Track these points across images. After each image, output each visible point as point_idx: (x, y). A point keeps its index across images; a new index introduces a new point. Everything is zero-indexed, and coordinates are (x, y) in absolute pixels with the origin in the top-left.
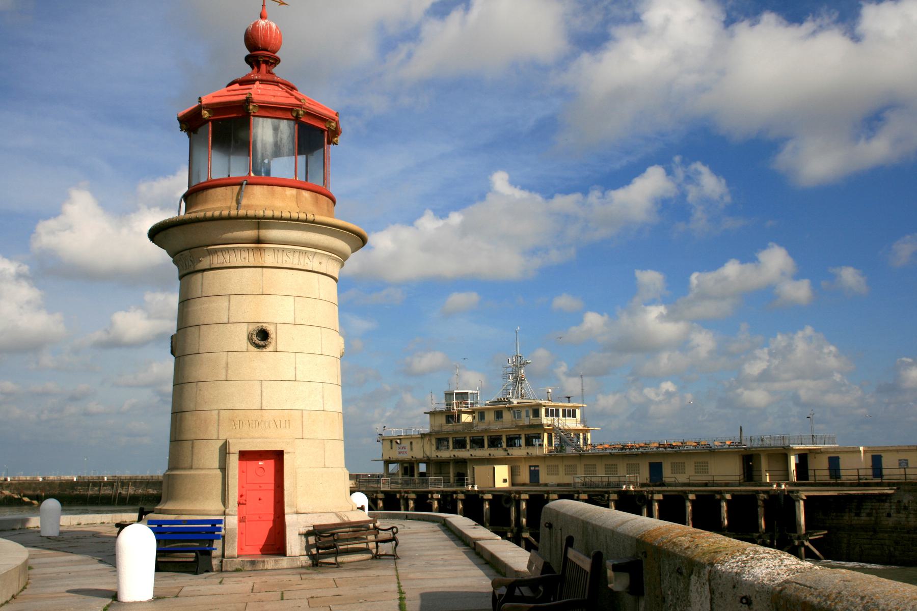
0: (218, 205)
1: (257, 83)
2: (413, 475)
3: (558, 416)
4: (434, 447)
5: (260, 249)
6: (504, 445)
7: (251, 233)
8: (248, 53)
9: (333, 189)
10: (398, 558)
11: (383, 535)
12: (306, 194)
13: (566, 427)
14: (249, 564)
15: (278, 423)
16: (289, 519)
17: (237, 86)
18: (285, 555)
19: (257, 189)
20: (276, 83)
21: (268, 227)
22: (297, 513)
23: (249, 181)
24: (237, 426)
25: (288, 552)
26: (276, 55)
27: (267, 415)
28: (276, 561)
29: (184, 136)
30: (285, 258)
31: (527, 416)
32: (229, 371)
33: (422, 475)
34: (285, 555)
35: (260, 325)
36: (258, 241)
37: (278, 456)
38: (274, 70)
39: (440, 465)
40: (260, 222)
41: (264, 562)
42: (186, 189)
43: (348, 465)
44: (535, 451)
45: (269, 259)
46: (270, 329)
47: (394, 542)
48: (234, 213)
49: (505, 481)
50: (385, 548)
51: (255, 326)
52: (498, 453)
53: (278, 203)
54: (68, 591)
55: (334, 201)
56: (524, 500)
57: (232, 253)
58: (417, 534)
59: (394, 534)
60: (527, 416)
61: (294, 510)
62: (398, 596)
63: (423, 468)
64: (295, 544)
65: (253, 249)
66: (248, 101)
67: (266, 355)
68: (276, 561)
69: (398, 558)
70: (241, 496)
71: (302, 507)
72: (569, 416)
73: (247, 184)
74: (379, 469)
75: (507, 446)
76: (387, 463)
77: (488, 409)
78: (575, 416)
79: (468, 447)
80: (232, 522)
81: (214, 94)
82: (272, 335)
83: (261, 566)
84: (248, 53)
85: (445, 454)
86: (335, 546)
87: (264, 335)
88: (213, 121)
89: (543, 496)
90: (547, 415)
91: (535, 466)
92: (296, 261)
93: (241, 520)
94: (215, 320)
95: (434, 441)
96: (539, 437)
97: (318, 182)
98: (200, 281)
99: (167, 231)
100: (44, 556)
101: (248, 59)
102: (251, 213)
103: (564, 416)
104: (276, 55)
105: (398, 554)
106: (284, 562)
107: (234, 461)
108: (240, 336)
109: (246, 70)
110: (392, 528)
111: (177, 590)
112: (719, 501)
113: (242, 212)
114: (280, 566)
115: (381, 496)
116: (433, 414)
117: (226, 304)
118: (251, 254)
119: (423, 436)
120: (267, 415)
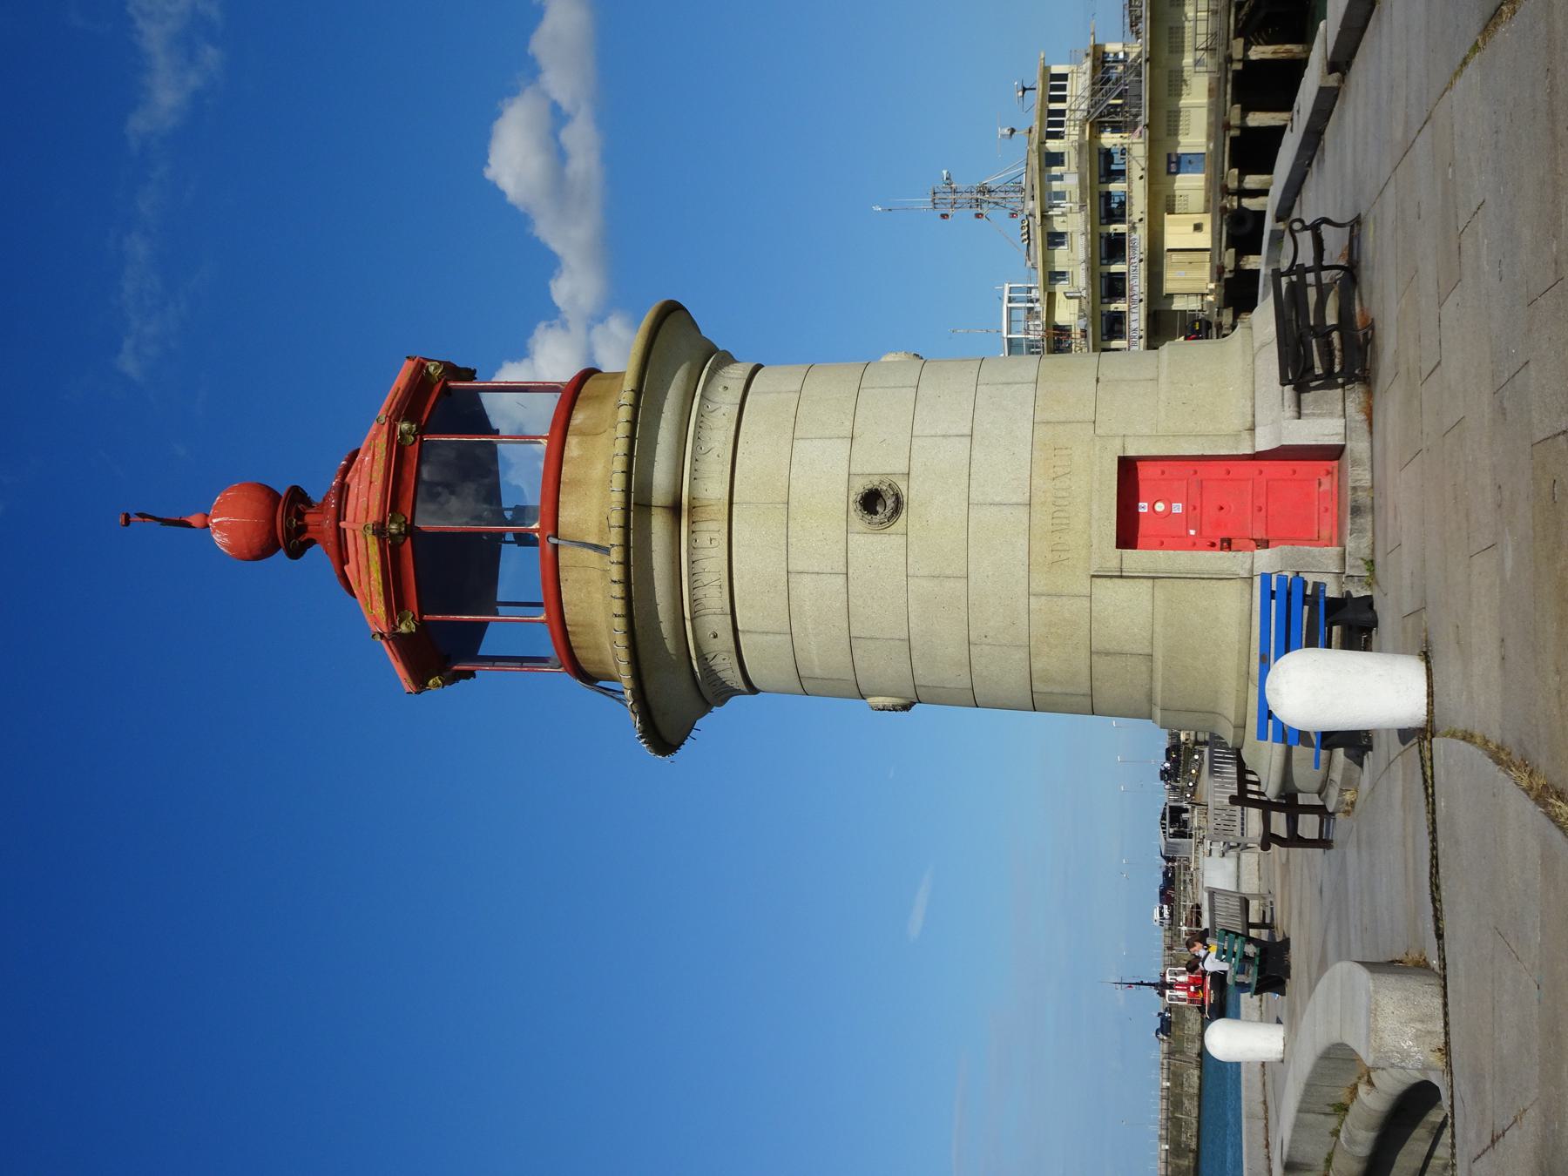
0: (598, 596)
1: (342, 524)
3: (1062, 113)
5: (692, 508)
6: (1121, 228)
7: (659, 524)
8: (282, 552)
12: (578, 418)
13: (1087, 94)
14: (1360, 521)
15: (1060, 471)
16: (1264, 443)
17: (350, 570)
18: (1343, 447)
19: (566, 516)
20: (343, 489)
21: (646, 487)
22: (1252, 429)
23: (549, 533)
26: (283, 493)
28: (1355, 463)
30: (712, 456)
31: (1060, 178)
32: (948, 572)
34: (1343, 447)
35: (852, 507)
36: (675, 509)
37: (1128, 468)
38: (316, 496)
40: (636, 503)
41: (1355, 489)
44: (1137, 166)
45: (713, 489)
46: (860, 486)
48: (616, 555)
49: (1198, 227)
50: (1334, 241)
51: (856, 516)
52: (1139, 240)
53: (598, 471)
56: (1241, 181)
57: (698, 568)
59: (1305, 228)
60: (1060, 178)
61: (1246, 435)
64: (1322, 424)
65: (692, 522)
66: (380, 530)
67: (914, 494)
68: (1355, 463)
70: (1213, 545)
71: (1237, 422)
72: (1063, 88)
73: (556, 536)
75: (1123, 222)
78: (1064, 77)
79: (1121, 228)
80: (1266, 560)
82: (874, 482)
83: (1363, 498)
84: (282, 552)
87: (870, 501)
88: (421, 613)
89: (1236, 72)
90: (1057, 136)
92: (713, 526)
93: (1264, 544)
94: (839, 604)
96: (1107, 155)
98: (756, 637)
101: (296, 553)
102: (616, 518)
103: (1063, 99)
104: (283, 493)
105: (1348, 218)
106: (1359, 447)
107: (1134, 559)
108: (876, 547)
109: (317, 556)
112: (1245, 130)
113: (615, 537)
114: (1366, 455)
117: (806, 579)
118: (703, 526)
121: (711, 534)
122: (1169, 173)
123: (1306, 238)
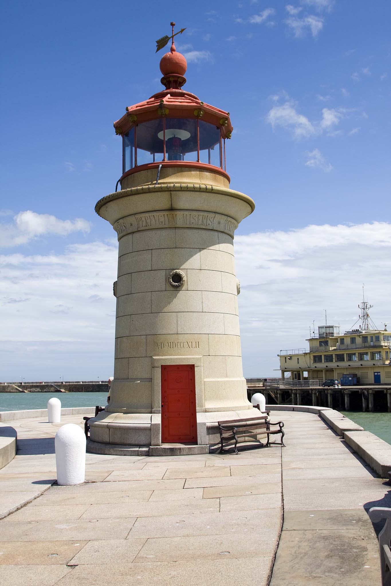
2: (299, 379)
4: (312, 361)
9: (227, 173)
10: (284, 446)
11: (273, 428)
12: (207, 174)
15: (190, 344)
22: (206, 411)
24: (160, 347)
25: (199, 441)
27: (181, 338)
29: (120, 138)
33: (305, 379)
39: (315, 373)
40: (170, 190)
42: (120, 175)
43: (244, 375)
47: (280, 435)
50: (273, 438)
54: (33, 483)
55: (229, 179)
58: (299, 423)
59: (281, 427)
62: (360, 312)
63: (306, 374)
69: (284, 446)
71: (208, 405)
74: (278, 375)
76: (283, 372)
77: (347, 336)
79: (334, 360)
81: (137, 105)
82: (185, 279)
85: (322, 365)
86: (233, 438)
89: (383, 391)
91: (378, 373)
95: (312, 358)
97: (215, 165)
99: (107, 205)
100: (121, 418)
104: (184, 76)
109: (162, 88)
110: (279, 423)
111: (107, 474)
112: (386, 395)
115: (279, 392)
116: (311, 340)
117: (150, 256)
119: (306, 354)
120: (181, 338)
121: (162, 218)
122: (374, 373)
123: (277, 428)
